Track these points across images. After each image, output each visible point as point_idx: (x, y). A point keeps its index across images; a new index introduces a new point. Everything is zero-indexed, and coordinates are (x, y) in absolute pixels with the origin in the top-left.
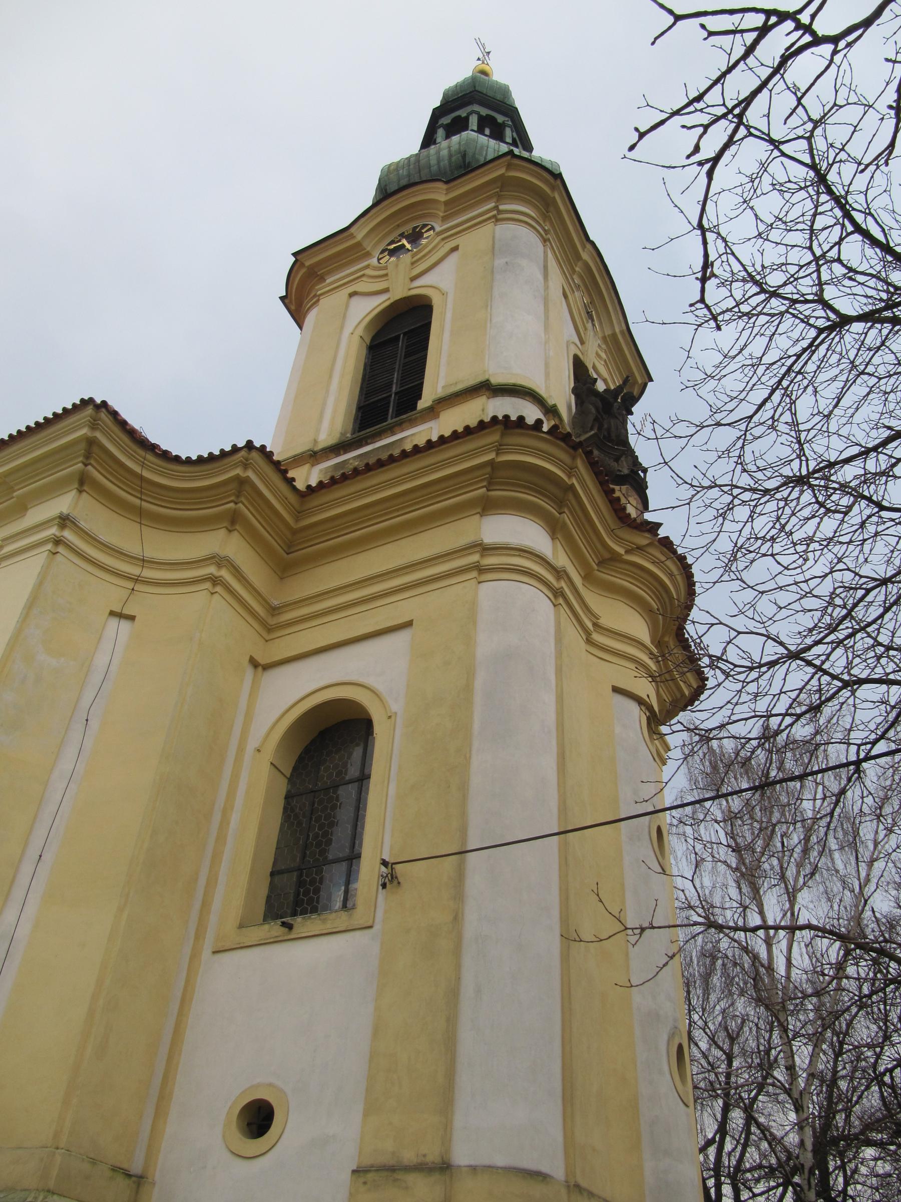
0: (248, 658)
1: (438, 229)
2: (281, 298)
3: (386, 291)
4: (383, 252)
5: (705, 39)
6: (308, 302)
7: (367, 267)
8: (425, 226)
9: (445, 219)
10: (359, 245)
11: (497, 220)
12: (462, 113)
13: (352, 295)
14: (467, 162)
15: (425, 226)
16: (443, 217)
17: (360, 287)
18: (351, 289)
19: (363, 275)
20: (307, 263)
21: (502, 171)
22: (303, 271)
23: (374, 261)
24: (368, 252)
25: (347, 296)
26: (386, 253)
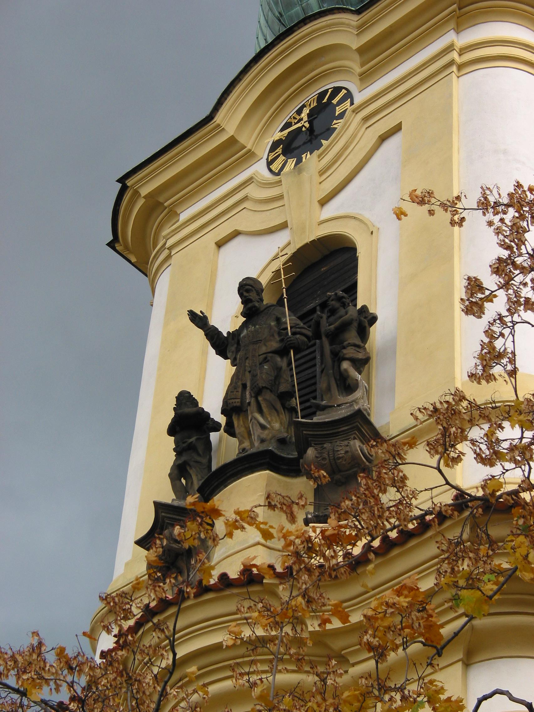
0: (238, 507)
2: (108, 244)
3: (284, 226)
10: (232, 141)
14: (347, 384)
15: (337, 90)
16: (361, 75)
19: (246, 198)
20: (144, 191)
22: (141, 202)
24: (250, 151)
26: (279, 150)
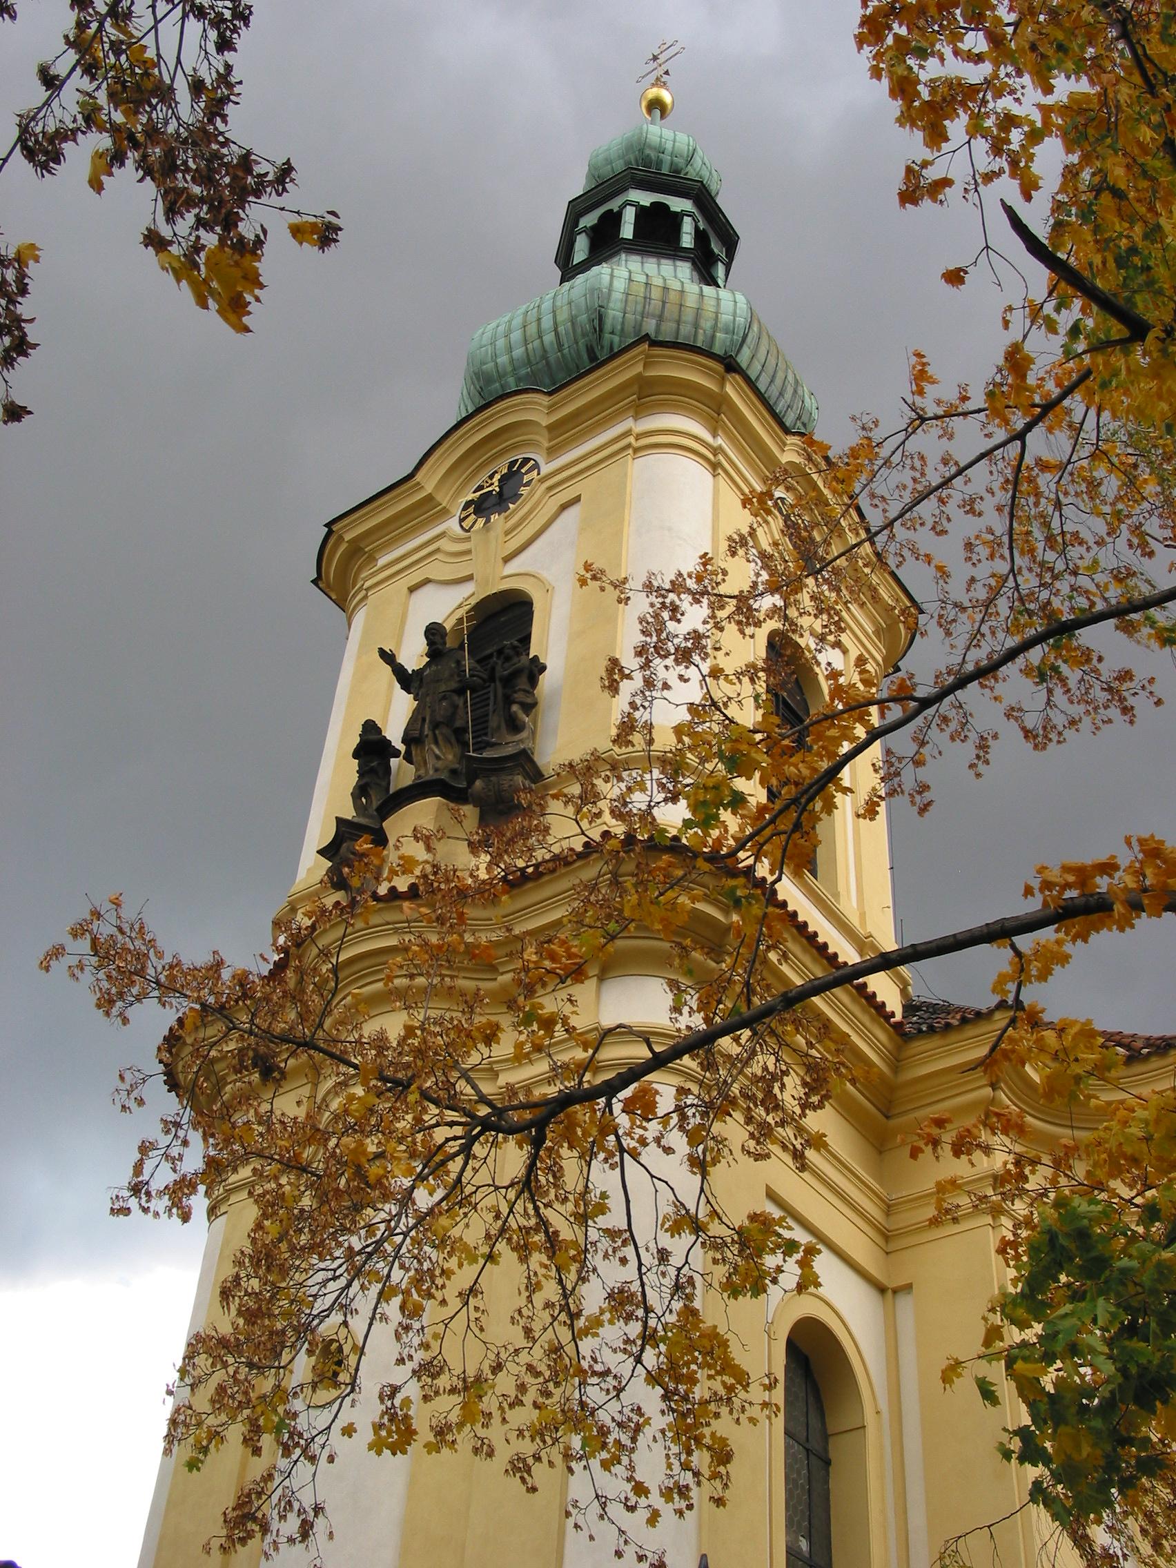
1: (546, 469)
4: (466, 508)
5: (388, 657)
6: (354, 596)
7: (442, 535)
8: (526, 460)
9: (552, 452)
10: (429, 498)
11: (636, 450)
12: (614, 205)
13: (412, 590)
15: (526, 460)
17: (434, 569)
18: (415, 577)
19: (438, 550)
20: (348, 537)
21: (639, 368)
23: (452, 525)
25: (405, 590)
26: (471, 510)
